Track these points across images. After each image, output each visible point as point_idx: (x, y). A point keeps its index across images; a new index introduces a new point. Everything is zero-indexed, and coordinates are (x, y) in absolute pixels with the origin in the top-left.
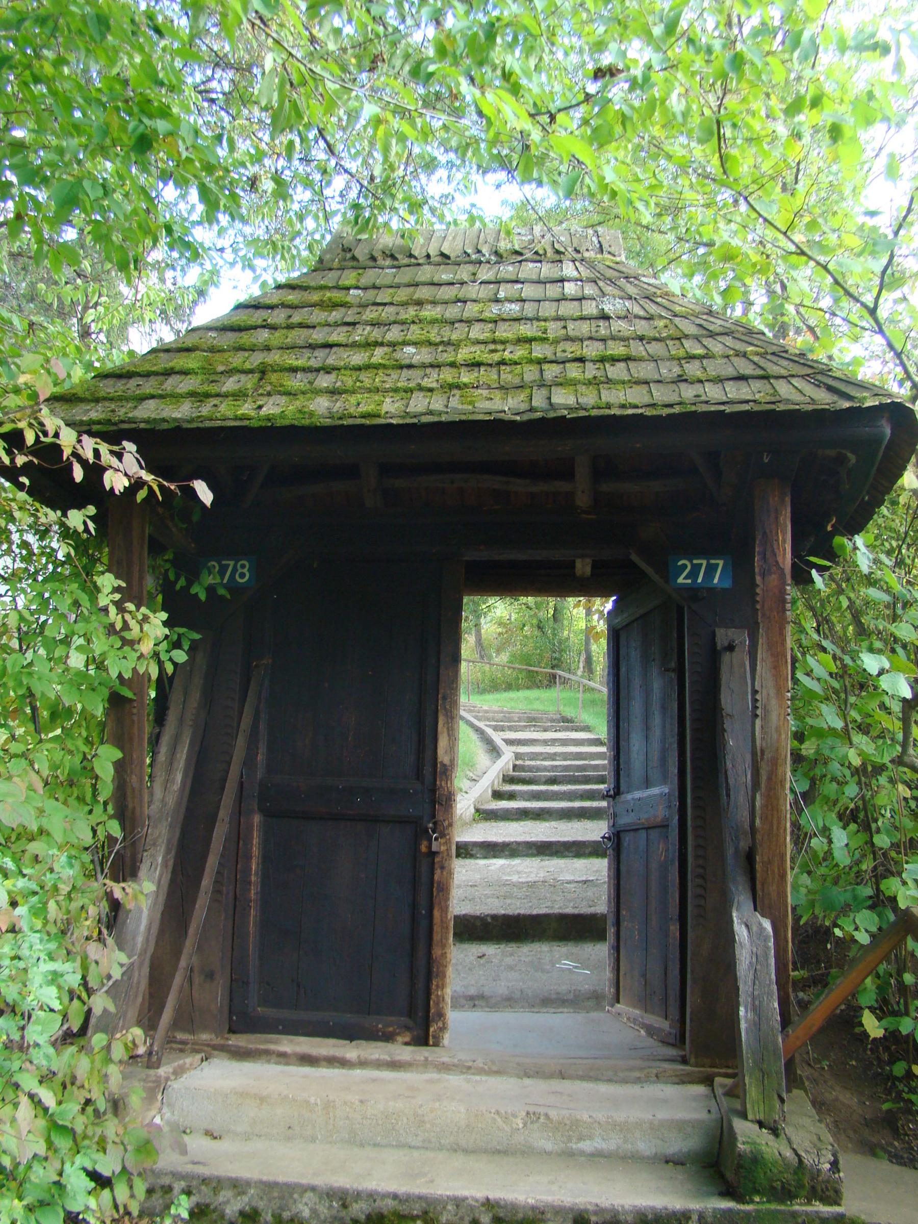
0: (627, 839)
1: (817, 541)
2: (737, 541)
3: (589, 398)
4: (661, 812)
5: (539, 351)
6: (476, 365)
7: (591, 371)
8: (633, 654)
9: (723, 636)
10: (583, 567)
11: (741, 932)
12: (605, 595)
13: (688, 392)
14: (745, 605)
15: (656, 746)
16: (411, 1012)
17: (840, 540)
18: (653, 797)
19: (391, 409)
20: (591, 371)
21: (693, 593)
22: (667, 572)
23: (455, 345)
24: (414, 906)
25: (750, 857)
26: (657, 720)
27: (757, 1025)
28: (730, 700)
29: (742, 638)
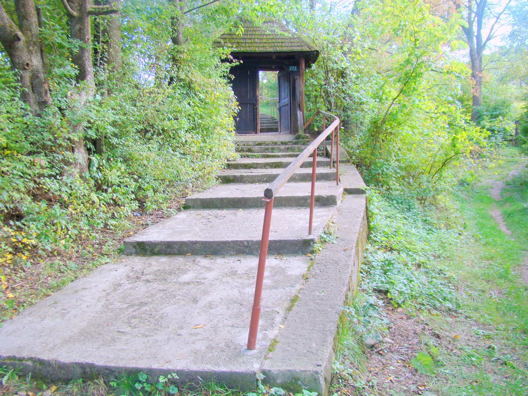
0: (282, 108)
1: (308, 66)
2: (298, 65)
3: (281, 49)
4: (287, 103)
5: (274, 41)
6: (266, 43)
7: (281, 44)
8: (282, 81)
9: (296, 77)
10: (273, 67)
11: (298, 114)
12: (276, 71)
13: (292, 48)
14: (298, 73)
15: (286, 94)
16: (254, 130)
17: (312, 64)
18: (286, 101)
19: (257, 50)
20: (281, 44)
21: (292, 71)
22: (288, 69)
23: (262, 39)
24: (254, 116)
25: (299, 105)
26: (286, 90)
27: (300, 124)
28: (297, 86)
29: (298, 77)
